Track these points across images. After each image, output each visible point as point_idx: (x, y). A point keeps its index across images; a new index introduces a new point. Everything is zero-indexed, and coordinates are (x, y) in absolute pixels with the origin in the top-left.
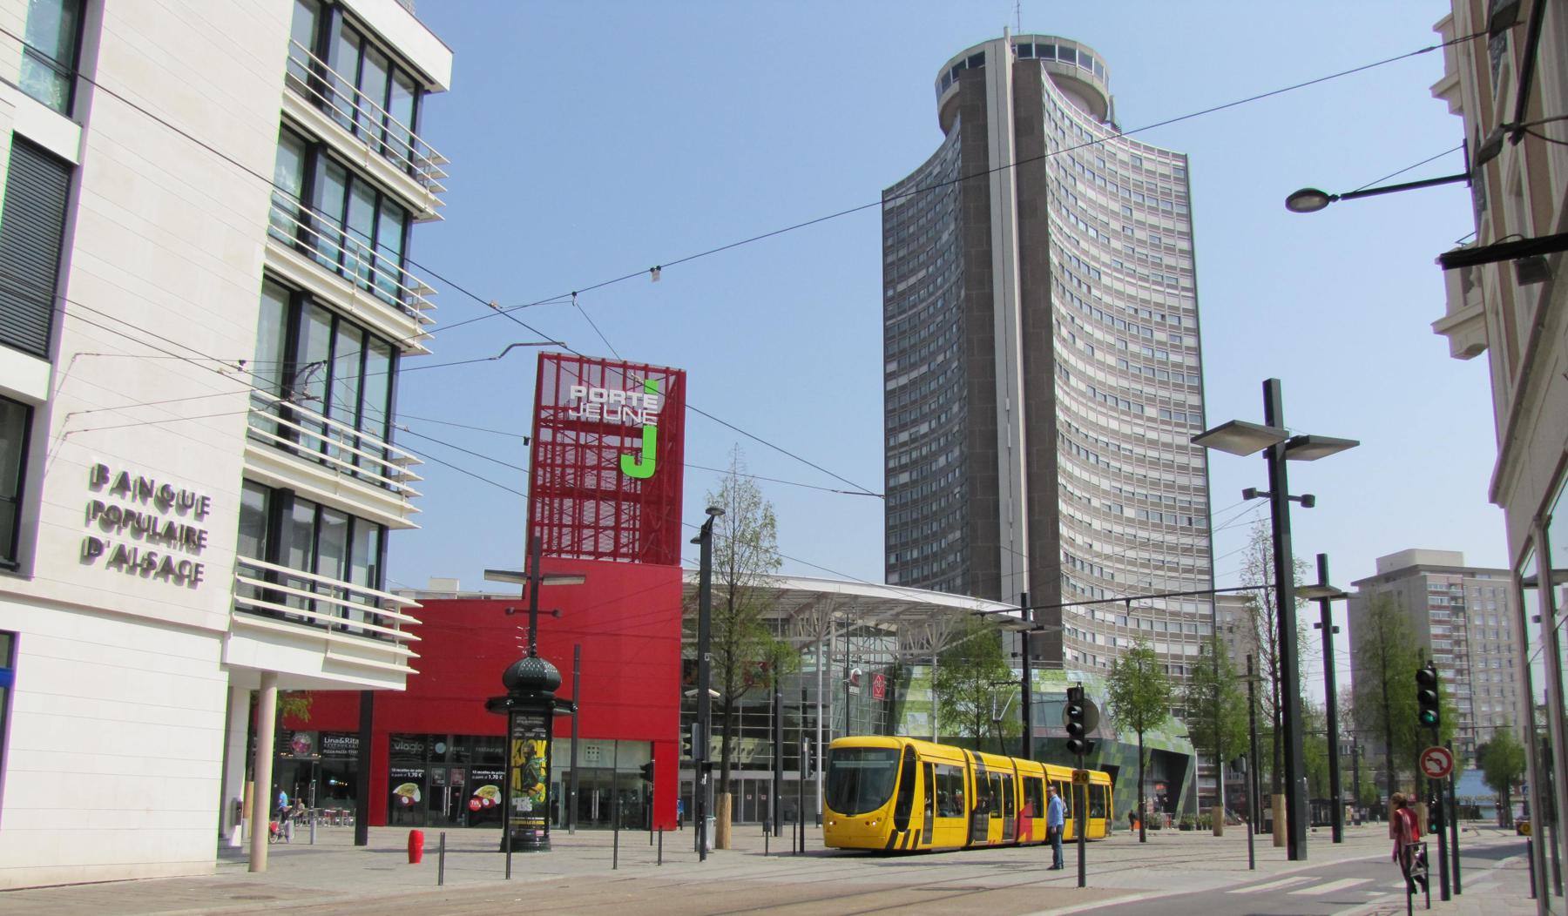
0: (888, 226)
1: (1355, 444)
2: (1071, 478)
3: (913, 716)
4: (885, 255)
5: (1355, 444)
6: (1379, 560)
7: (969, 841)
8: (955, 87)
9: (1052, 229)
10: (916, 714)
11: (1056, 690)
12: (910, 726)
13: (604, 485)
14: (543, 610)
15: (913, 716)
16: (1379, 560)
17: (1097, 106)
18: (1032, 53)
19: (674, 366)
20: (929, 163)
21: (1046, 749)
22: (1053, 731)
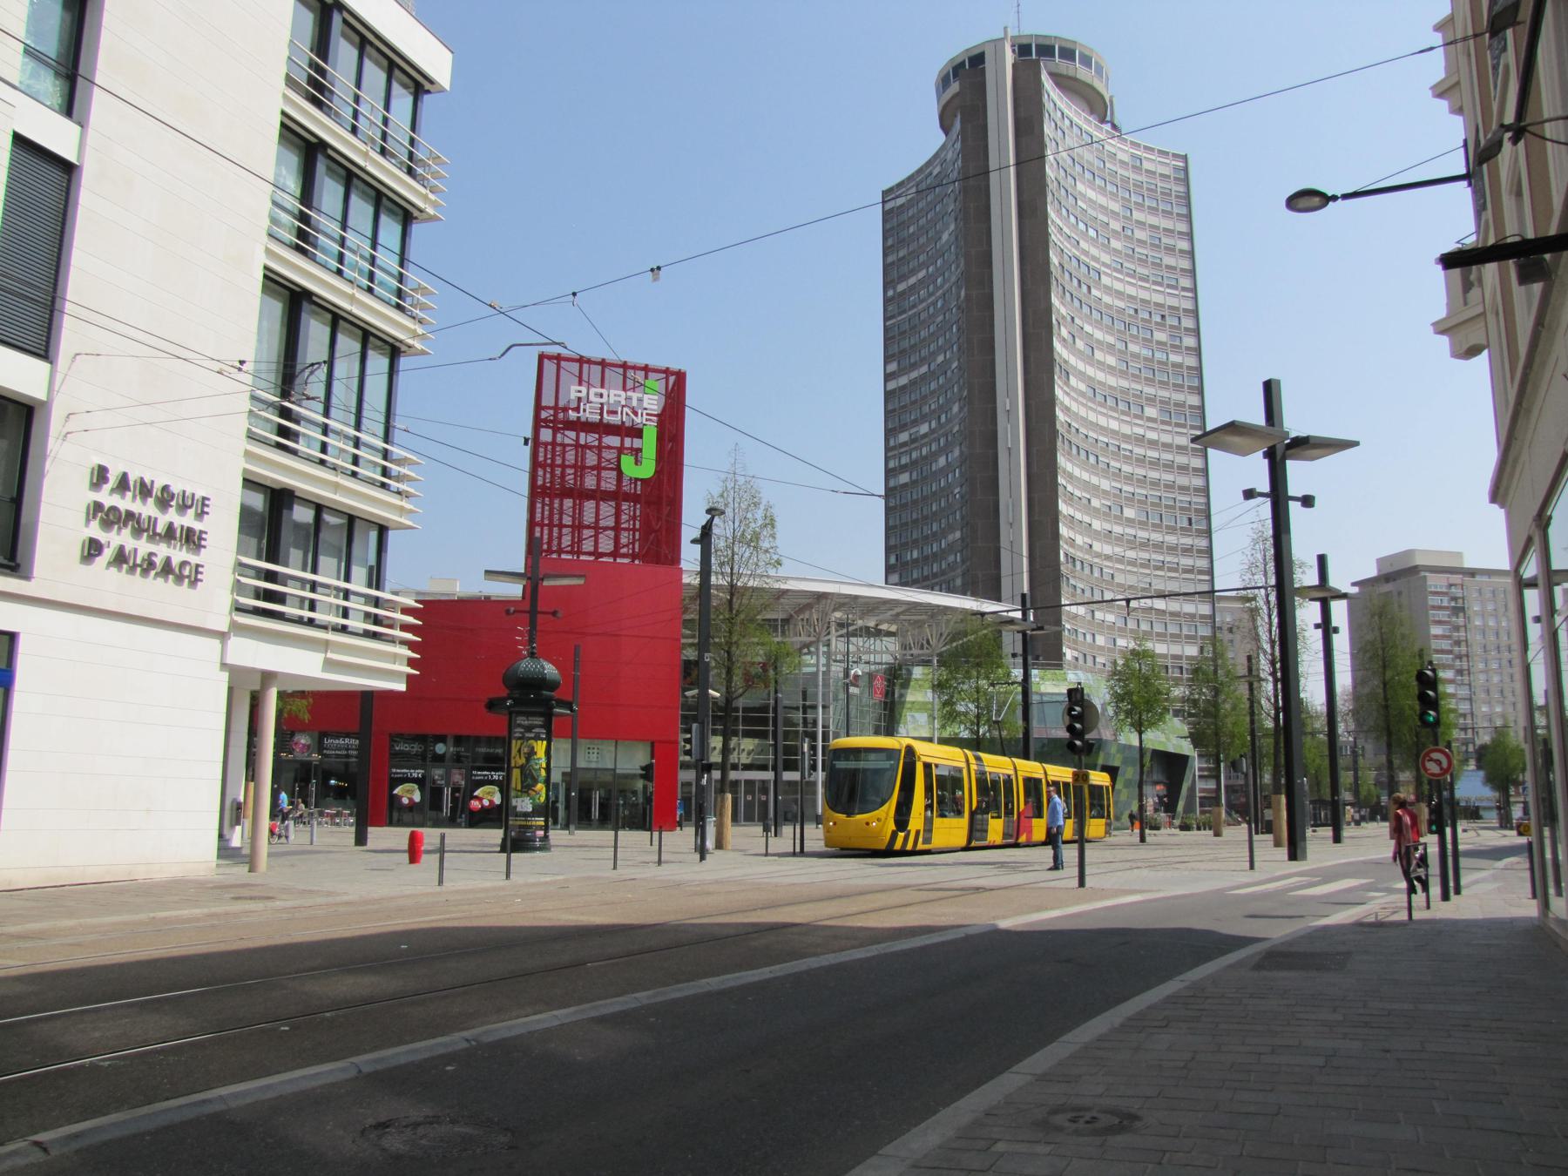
3: (913, 716)
4: (885, 255)
8: (955, 87)
9: (1052, 229)
10: (916, 715)
15: (913, 716)
18: (1032, 53)
19: (674, 367)
20: (929, 163)
21: (1046, 749)
22: (1053, 731)
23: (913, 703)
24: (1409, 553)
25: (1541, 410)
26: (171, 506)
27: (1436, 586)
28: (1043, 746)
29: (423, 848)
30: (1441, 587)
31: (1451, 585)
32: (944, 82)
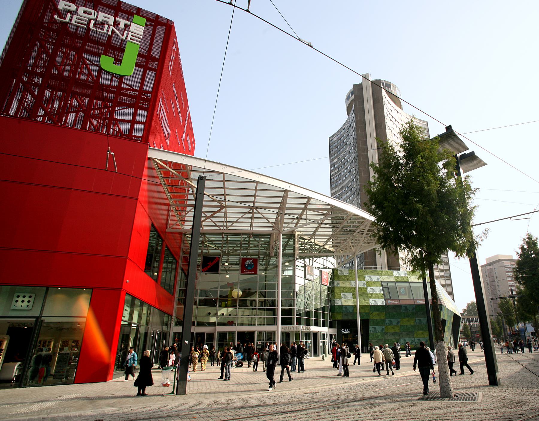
0: (331, 148)
1: (454, 301)
2: (391, 397)
3: (344, 295)
4: (330, 146)
5: (454, 301)
6: (486, 259)
7: (385, 288)
8: (352, 98)
9: (388, 131)
10: (346, 294)
11: (403, 368)
12: (343, 300)
13: (168, 267)
14: (39, 313)
15: (344, 295)
16: (486, 259)
17: (396, 99)
18: (377, 85)
19: (164, 13)
20: (344, 125)
21: (414, 311)
22: (418, 301)
23: (344, 287)
24: (497, 256)
25: (257, 406)
26: (350, 354)
27: (507, 265)
28: (413, 309)
29: (527, 323)
30: (509, 265)
31: (512, 265)
32: (348, 97)
